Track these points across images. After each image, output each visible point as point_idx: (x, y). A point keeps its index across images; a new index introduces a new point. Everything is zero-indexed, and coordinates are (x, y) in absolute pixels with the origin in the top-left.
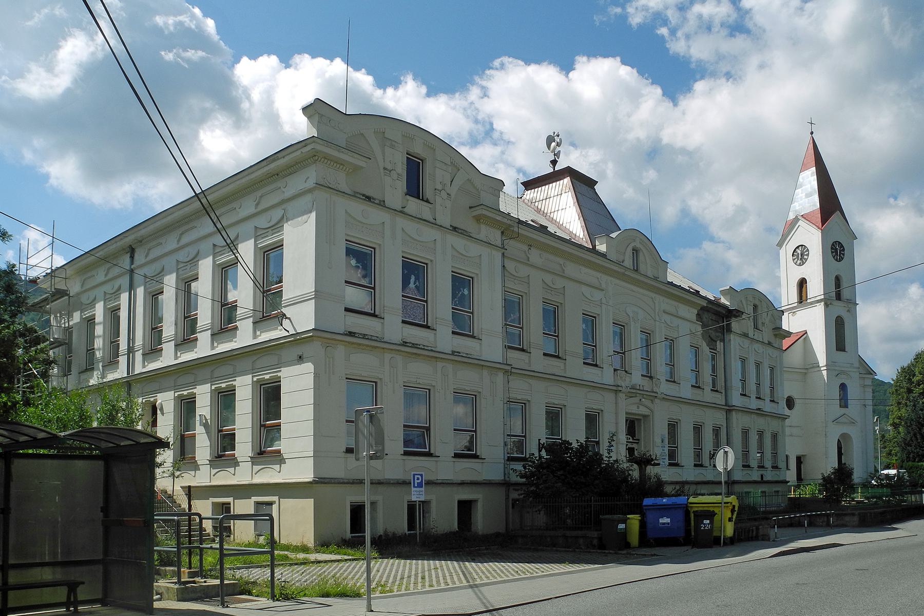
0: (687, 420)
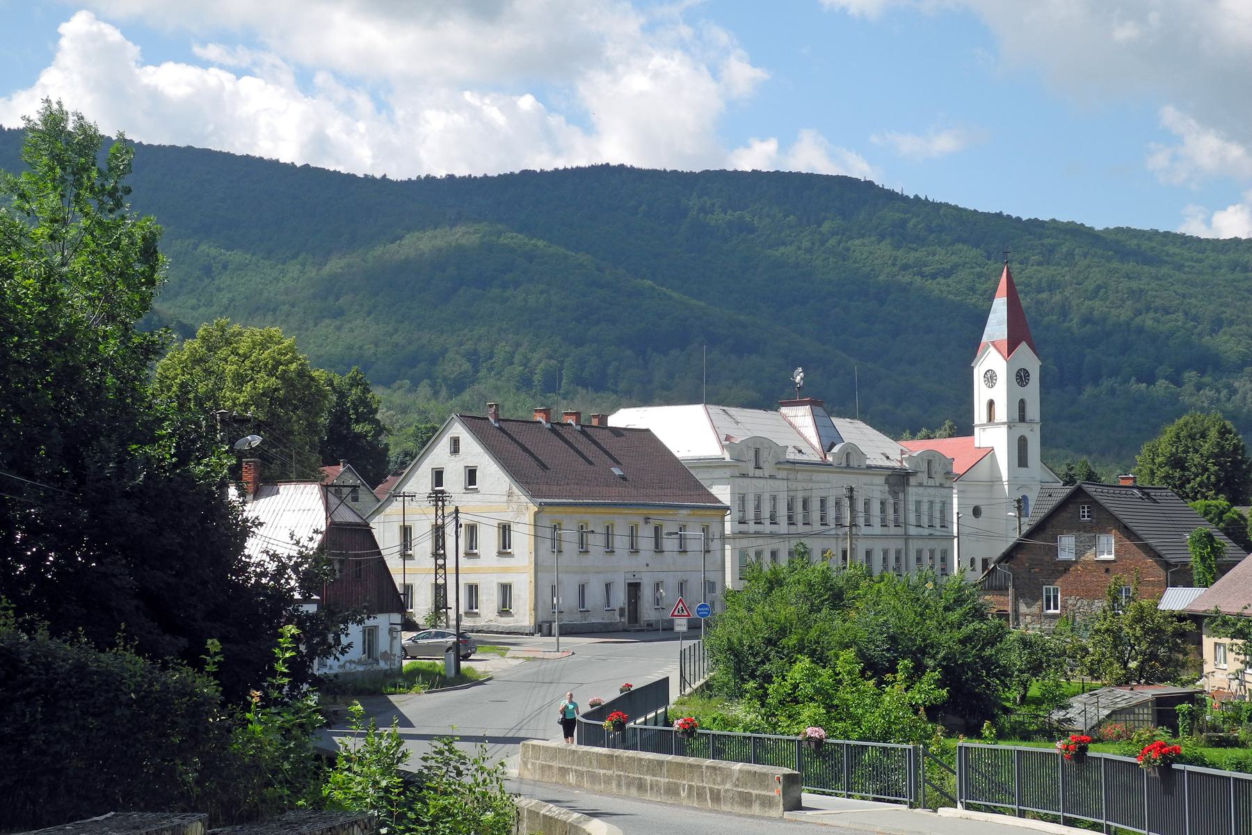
0: (878, 548)
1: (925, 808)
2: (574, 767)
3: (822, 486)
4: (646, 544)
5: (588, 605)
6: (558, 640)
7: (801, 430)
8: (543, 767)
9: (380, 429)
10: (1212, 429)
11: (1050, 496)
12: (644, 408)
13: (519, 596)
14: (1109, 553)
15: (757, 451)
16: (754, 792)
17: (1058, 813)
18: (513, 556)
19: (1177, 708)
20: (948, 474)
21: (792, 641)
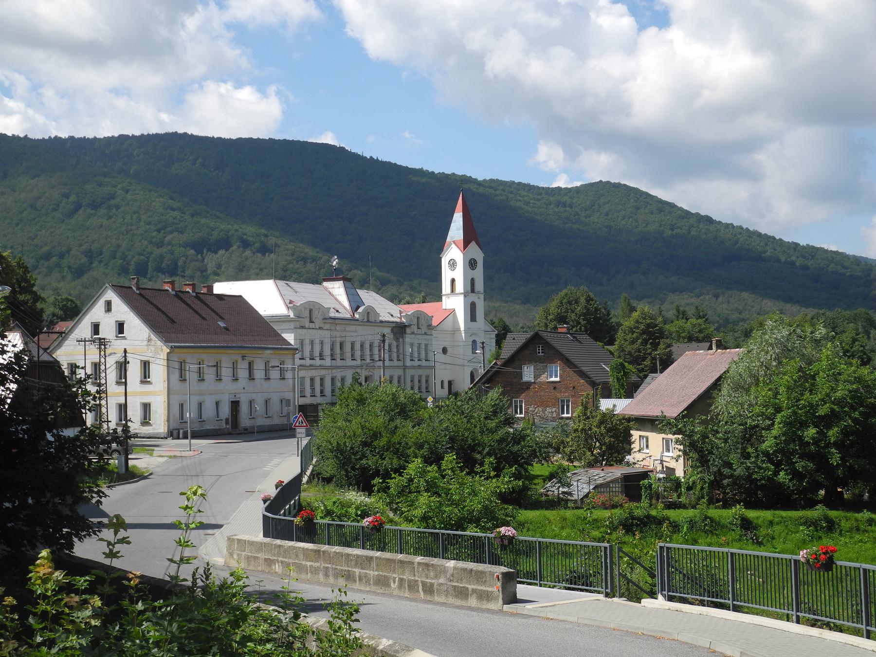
1: (620, 597)
2: (280, 559)
3: (352, 334)
4: (243, 374)
5: (204, 417)
6: (190, 443)
7: (337, 297)
8: (248, 558)
9: (37, 298)
10: (582, 298)
11: (514, 339)
12: (233, 282)
13: (156, 412)
14: (556, 376)
15: (311, 311)
16: (470, 587)
17: (859, 626)
18: (151, 384)
19: (641, 483)
20: (430, 326)
21: (383, 442)
